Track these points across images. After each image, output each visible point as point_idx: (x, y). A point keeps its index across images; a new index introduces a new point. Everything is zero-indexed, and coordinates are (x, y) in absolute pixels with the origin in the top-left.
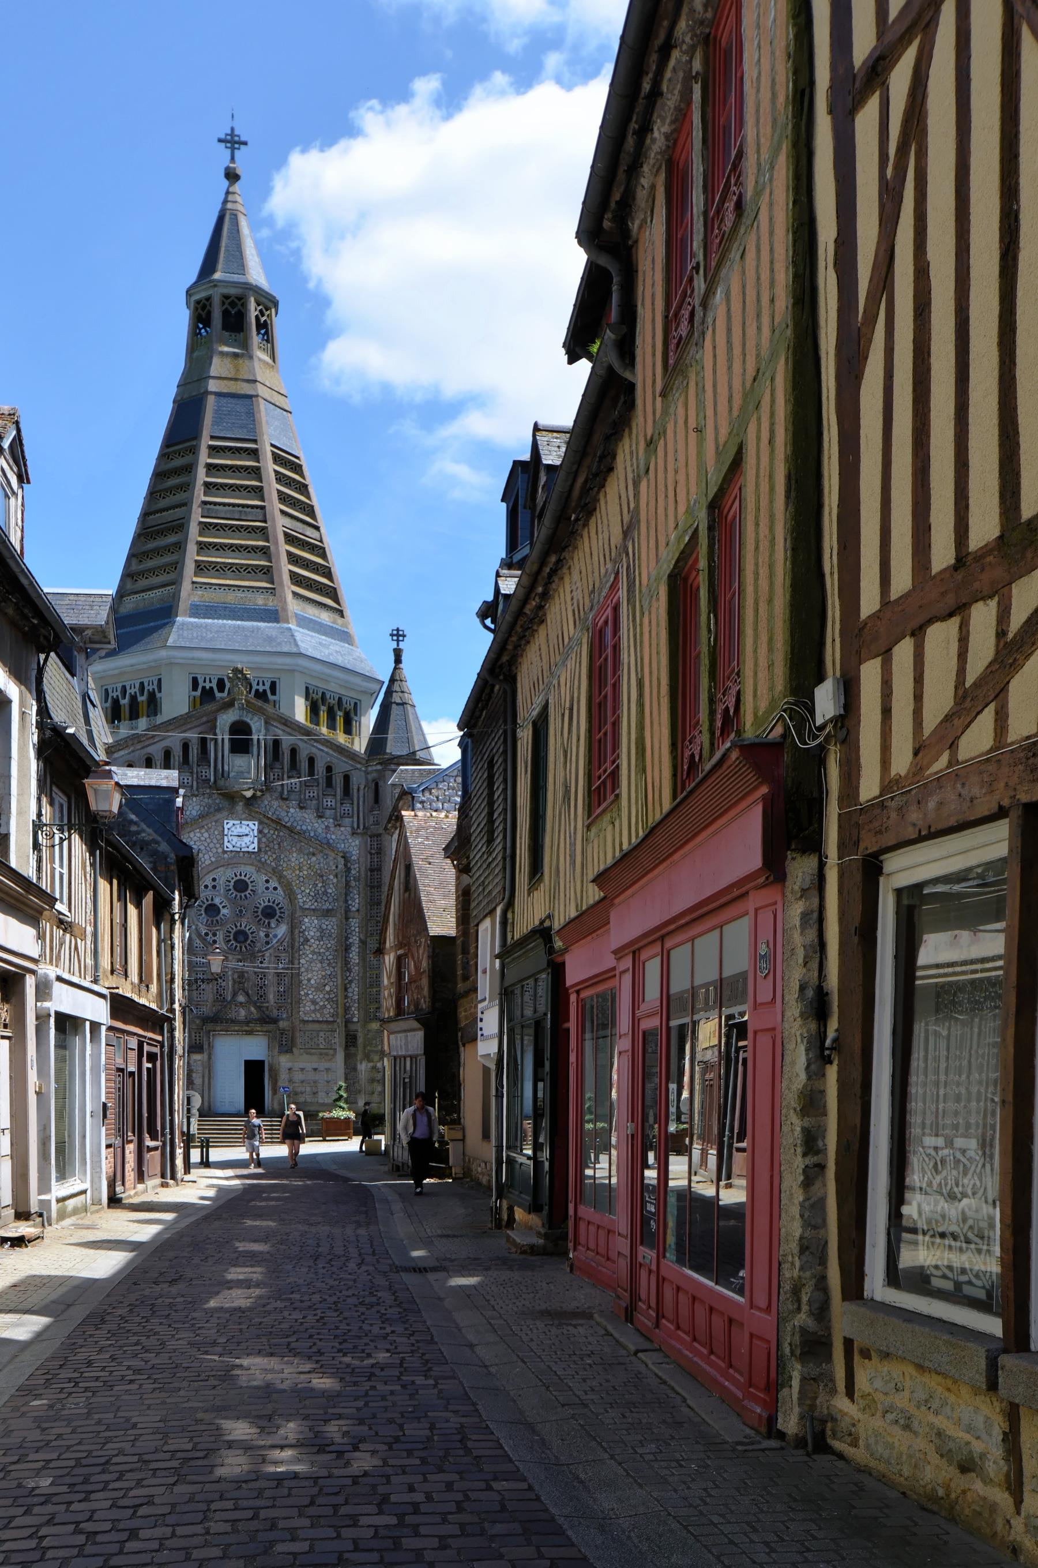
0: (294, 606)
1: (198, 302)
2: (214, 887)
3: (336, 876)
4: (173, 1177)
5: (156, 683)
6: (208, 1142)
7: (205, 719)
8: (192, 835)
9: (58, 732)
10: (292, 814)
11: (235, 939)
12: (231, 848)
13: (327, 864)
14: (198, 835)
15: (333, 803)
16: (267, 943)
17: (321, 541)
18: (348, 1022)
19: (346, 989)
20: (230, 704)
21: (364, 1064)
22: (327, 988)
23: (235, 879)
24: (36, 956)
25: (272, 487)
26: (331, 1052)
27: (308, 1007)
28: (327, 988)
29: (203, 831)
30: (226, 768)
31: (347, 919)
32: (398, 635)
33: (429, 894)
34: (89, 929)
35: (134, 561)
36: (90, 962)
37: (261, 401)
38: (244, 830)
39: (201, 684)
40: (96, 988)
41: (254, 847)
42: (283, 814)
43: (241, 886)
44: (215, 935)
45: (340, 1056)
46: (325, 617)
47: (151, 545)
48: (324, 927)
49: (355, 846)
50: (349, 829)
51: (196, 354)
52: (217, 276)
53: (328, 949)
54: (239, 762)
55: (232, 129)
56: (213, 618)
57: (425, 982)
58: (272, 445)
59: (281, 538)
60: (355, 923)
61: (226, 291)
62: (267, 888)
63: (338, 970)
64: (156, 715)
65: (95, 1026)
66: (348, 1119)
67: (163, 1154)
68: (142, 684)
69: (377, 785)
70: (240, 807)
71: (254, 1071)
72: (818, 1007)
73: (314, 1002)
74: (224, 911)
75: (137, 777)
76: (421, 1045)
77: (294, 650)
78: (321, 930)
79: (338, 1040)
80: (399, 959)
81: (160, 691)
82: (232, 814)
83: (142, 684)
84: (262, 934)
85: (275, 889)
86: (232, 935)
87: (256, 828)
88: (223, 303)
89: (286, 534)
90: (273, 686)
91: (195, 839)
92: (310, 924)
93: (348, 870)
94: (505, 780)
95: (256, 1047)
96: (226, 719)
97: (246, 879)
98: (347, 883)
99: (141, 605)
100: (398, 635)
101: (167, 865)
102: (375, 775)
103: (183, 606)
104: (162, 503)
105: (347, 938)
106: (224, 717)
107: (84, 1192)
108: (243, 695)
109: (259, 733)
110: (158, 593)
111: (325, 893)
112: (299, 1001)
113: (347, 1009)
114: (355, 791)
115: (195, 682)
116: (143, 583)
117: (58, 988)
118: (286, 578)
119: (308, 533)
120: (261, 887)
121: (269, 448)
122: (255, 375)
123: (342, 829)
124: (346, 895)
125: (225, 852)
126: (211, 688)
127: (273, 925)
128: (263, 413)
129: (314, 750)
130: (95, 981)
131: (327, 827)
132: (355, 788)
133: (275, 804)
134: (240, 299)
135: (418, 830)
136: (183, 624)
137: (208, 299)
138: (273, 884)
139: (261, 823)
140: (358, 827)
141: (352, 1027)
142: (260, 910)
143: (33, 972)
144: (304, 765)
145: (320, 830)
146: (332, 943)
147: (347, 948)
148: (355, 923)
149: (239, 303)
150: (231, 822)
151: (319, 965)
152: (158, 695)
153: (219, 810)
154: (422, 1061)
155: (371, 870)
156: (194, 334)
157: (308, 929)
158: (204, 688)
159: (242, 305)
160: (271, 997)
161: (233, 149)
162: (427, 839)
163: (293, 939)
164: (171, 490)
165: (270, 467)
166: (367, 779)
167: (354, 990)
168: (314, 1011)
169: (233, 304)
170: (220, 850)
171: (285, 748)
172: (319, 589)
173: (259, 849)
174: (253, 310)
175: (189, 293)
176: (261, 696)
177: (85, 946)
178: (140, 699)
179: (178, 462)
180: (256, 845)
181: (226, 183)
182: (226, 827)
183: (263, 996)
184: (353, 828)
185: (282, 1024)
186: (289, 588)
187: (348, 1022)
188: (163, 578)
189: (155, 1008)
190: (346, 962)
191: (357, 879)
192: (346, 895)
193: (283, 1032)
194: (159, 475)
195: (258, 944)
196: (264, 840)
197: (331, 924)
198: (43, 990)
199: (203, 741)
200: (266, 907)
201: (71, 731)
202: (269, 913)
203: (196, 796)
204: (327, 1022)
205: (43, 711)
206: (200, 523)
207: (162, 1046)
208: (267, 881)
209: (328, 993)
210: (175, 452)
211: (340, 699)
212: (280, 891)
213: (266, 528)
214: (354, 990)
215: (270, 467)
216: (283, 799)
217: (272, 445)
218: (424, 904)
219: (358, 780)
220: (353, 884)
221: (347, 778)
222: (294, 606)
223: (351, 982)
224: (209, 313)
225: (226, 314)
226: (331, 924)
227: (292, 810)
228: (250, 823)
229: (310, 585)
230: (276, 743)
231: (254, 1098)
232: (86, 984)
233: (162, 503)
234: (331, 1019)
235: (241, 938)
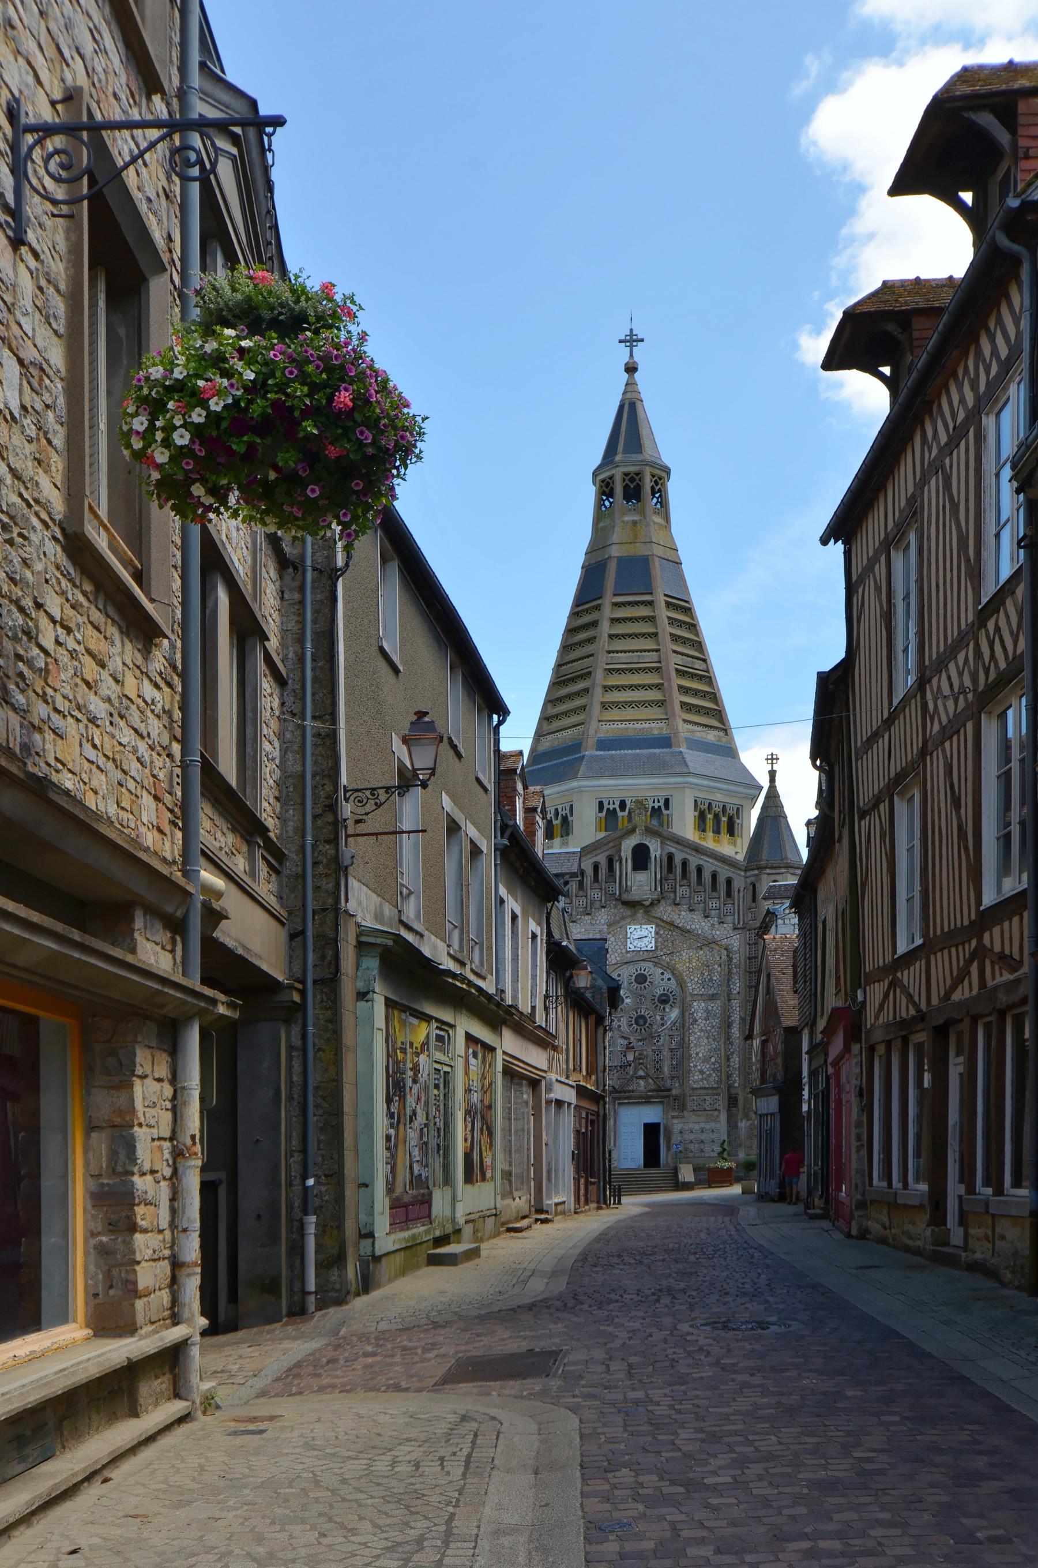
0: (683, 729)
1: (603, 481)
3: (720, 965)
4: (605, 1203)
5: (568, 808)
6: (619, 1189)
7: (611, 844)
9: (558, 944)
10: (683, 917)
11: (637, 1023)
12: (633, 949)
13: (713, 956)
16: (663, 1025)
17: (707, 671)
18: (730, 1087)
19: (728, 1060)
20: (633, 831)
21: (744, 1121)
22: (713, 1060)
24: (545, 1068)
25: (666, 630)
26: (716, 1113)
27: (697, 1076)
28: (713, 1060)
30: (629, 883)
31: (729, 1000)
33: (783, 996)
34: (564, 1047)
35: (549, 706)
36: (564, 1066)
37: (655, 558)
38: (644, 933)
39: (606, 806)
40: (567, 1081)
41: (652, 946)
42: (676, 917)
43: (641, 979)
44: (619, 1021)
45: (723, 1116)
46: (711, 736)
47: (564, 691)
48: (710, 1008)
49: (736, 942)
50: (731, 925)
51: (601, 525)
52: (618, 457)
53: (713, 1027)
54: (641, 877)
55: (631, 330)
56: (616, 750)
57: (779, 1060)
58: (665, 595)
59: (673, 673)
60: (735, 1003)
61: (626, 470)
63: (722, 1043)
64: (568, 835)
65: (569, 1104)
66: (730, 1169)
67: (599, 1187)
68: (557, 810)
69: (754, 886)
70: (640, 913)
71: (651, 1132)
72: (860, 1094)
73: (701, 1072)
74: (628, 1001)
75: (580, 933)
76: (777, 1106)
77: (685, 770)
78: (707, 1011)
79: (722, 1103)
80: (764, 1043)
81: (572, 815)
82: (634, 919)
83: (557, 810)
84: (658, 1018)
85: (669, 979)
87: (653, 931)
88: (624, 480)
89: (677, 670)
90: (667, 802)
92: (698, 1008)
93: (730, 959)
94: (811, 950)
95: (652, 1114)
96: (628, 845)
98: (730, 972)
99: (556, 743)
101: (602, 994)
102: (753, 879)
103: (591, 742)
104: (573, 655)
105: (729, 1017)
106: (628, 842)
107: (564, 1203)
108: (641, 820)
109: (655, 849)
110: (570, 732)
111: (711, 980)
112: (689, 1072)
113: (729, 1076)
115: (601, 805)
116: (557, 724)
117: (557, 1087)
118: (677, 707)
119: (696, 667)
121: (663, 599)
122: (650, 537)
124: (728, 980)
125: (628, 952)
126: (615, 809)
127: (667, 1010)
128: (658, 569)
130: (567, 1078)
131: (713, 925)
132: (736, 890)
133: (669, 909)
134: (637, 474)
135: (776, 949)
136: (592, 756)
137: (611, 477)
138: (667, 976)
139: (657, 926)
141: (733, 1091)
143: (544, 1078)
144: (693, 876)
145: (706, 928)
146: (716, 1022)
147: (729, 1026)
148: (735, 1003)
149: (637, 478)
150: (633, 927)
151: (706, 1041)
152: (570, 819)
153: (623, 918)
154: (778, 1118)
155: (750, 958)
156: (599, 504)
157: (696, 1011)
158: (608, 809)
159: (640, 480)
160: (666, 1069)
161: (631, 347)
162: (782, 955)
163: (684, 1020)
164: (580, 644)
165: (664, 614)
167: (735, 1060)
168: (702, 1080)
169: (632, 480)
170: (624, 951)
171: (678, 860)
172: (707, 712)
173: (656, 947)
174: (648, 483)
175: (595, 474)
176: (656, 812)
177: (562, 1057)
178: (555, 822)
179: (586, 619)
180: (653, 944)
181: (626, 376)
182: (629, 931)
183: (659, 1070)
184: (734, 924)
185: (674, 1092)
186: (680, 714)
187: (730, 1087)
188: (574, 719)
189: (593, 1088)
190: (728, 1037)
191: (738, 967)
192: (728, 980)
193: (676, 1098)
194: (570, 631)
195: (655, 1027)
196: (660, 939)
197: (715, 1006)
198: (549, 1089)
199: (610, 861)
200: (662, 995)
201: (564, 944)
202: (664, 1000)
203: (604, 907)
204: (713, 1088)
205: (549, 934)
206: (606, 669)
207: (598, 1115)
208: (663, 974)
209: (713, 1064)
210: (583, 611)
211: (724, 806)
212: (673, 981)
213: (661, 668)
214: (735, 1060)
215: (664, 614)
216: (676, 904)
217: (665, 595)
218: (779, 1005)
219: (739, 883)
220: (734, 971)
221: (729, 882)
222: (683, 729)
223: (732, 1053)
224: (612, 489)
225: (626, 488)
226: (715, 1006)
227: (683, 913)
228: (649, 927)
229: (698, 710)
230: (670, 857)
231: (652, 1157)
232: (563, 1079)
233: (573, 655)
234: (715, 1086)
235: (641, 1022)
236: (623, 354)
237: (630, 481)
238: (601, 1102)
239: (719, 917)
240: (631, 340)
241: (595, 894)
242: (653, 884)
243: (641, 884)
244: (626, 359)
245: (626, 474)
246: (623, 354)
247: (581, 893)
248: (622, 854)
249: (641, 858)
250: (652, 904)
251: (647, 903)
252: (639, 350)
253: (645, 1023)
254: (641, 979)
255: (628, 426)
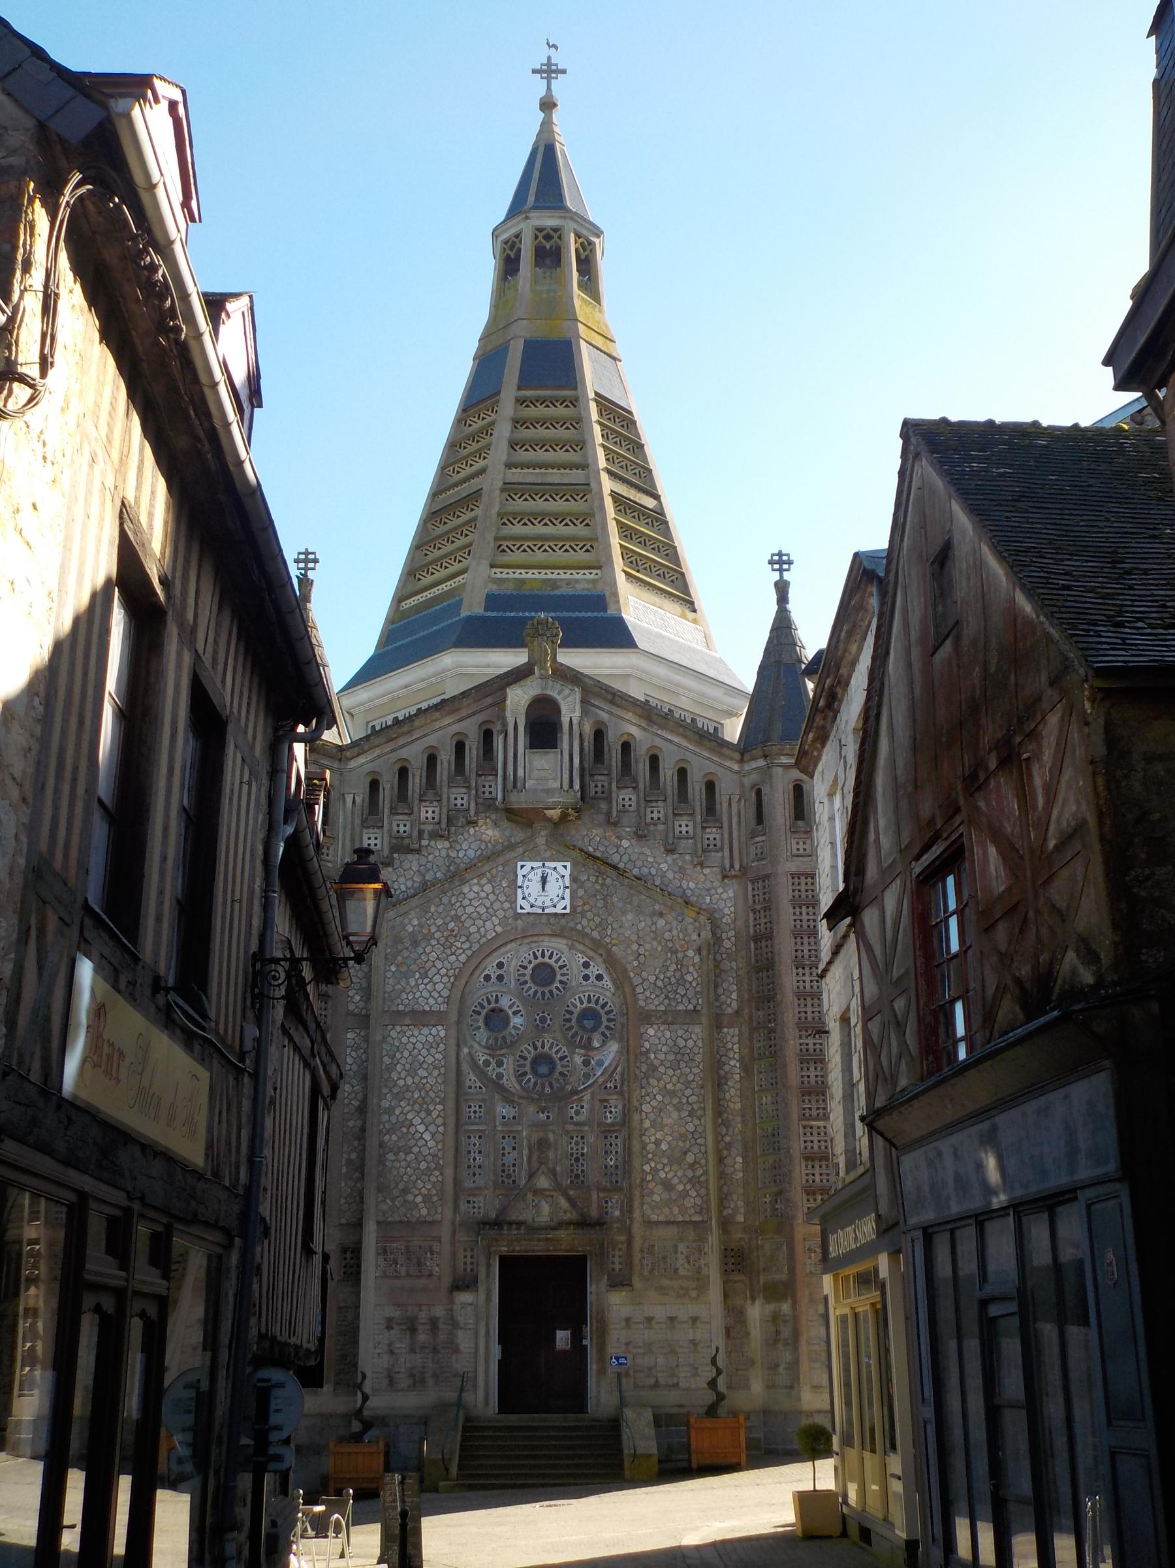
2: (500, 978)
8: (466, 889)
10: (625, 849)
12: (528, 909)
13: (685, 931)
14: (476, 888)
15: (690, 829)
22: (690, 1158)
23: (535, 962)
28: (690, 1158)
29: (484, 881)
30: (520, 772)
31: (719, 1027)
32: (780, 562)
41: (564, 906)
43: (544, 974)
53: (687, 1084)
62: (586, 978)
63: (708, 1120)
69: (759, 793)
73: (667, 1186)
74: (517, 1021)
78: (678, 1051)
84: (578, 1060)
85: (599, 977)
86: (528, 1063)
87: (567, 873)
88: (536, 237)
91: (471, 895)
93: (717, 940)
97: (552, 962)
100: (780, 562)
102: (755, 777)
114: (725, 805)
120: (575, 978)
123: (706, 871)
125: (518, 916)
129: (658, 742)
132: (725, 800)
134: (556, 230)
138: (594, 970)
140: (732, 866)
142: (574, 1017)
144: (642, 769)
146: (696, 1073)
147: (720, 1083)
149: (556, 235)
151: (675, 1115)
153: (511, 847)
155: (757, 939)
159: (560, 237)
161: (549, 79)
166: (742, 785)
169: (548, 237)
170: (510, 913)
171: (613, 740)
175: (495, 233)
180: (567, 902)
182: (520, 873)
184: (724, 869)
190: (719, 1111)
196: (581, 892)
199: (488, 736)
208: (586, 965)
209: (692, 1166)
212: (607, 982)
219: (726, 787)
221: (710, 786)
223: (729, 1145)
236: (538, 87)
237: (544, 242)
238: (930, 1231)
239: (694, 854)
240: (549, 71)
241: (459, 797)
242: (566, 776)
243: (546, 775)
244: (542, 93)
245: (540, 230)
246: (538, 87)
247: (430, 794)
248: (508, 714)
249: (543, 728)
250: (564, 816)
251: (555, 814)
252: (559, 87)
253: (552, 1069)
254: (544, 974)
255: (543, 178)
